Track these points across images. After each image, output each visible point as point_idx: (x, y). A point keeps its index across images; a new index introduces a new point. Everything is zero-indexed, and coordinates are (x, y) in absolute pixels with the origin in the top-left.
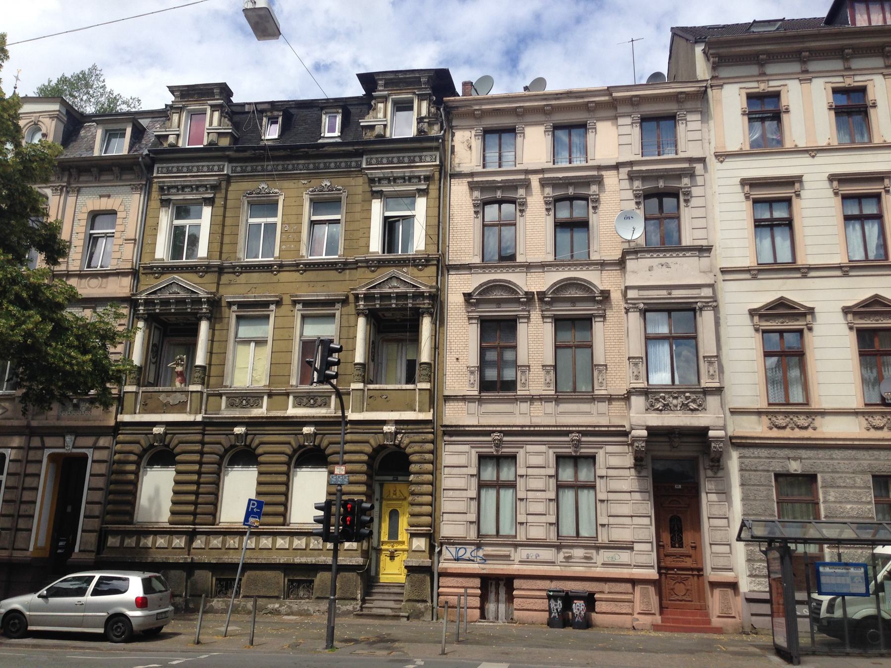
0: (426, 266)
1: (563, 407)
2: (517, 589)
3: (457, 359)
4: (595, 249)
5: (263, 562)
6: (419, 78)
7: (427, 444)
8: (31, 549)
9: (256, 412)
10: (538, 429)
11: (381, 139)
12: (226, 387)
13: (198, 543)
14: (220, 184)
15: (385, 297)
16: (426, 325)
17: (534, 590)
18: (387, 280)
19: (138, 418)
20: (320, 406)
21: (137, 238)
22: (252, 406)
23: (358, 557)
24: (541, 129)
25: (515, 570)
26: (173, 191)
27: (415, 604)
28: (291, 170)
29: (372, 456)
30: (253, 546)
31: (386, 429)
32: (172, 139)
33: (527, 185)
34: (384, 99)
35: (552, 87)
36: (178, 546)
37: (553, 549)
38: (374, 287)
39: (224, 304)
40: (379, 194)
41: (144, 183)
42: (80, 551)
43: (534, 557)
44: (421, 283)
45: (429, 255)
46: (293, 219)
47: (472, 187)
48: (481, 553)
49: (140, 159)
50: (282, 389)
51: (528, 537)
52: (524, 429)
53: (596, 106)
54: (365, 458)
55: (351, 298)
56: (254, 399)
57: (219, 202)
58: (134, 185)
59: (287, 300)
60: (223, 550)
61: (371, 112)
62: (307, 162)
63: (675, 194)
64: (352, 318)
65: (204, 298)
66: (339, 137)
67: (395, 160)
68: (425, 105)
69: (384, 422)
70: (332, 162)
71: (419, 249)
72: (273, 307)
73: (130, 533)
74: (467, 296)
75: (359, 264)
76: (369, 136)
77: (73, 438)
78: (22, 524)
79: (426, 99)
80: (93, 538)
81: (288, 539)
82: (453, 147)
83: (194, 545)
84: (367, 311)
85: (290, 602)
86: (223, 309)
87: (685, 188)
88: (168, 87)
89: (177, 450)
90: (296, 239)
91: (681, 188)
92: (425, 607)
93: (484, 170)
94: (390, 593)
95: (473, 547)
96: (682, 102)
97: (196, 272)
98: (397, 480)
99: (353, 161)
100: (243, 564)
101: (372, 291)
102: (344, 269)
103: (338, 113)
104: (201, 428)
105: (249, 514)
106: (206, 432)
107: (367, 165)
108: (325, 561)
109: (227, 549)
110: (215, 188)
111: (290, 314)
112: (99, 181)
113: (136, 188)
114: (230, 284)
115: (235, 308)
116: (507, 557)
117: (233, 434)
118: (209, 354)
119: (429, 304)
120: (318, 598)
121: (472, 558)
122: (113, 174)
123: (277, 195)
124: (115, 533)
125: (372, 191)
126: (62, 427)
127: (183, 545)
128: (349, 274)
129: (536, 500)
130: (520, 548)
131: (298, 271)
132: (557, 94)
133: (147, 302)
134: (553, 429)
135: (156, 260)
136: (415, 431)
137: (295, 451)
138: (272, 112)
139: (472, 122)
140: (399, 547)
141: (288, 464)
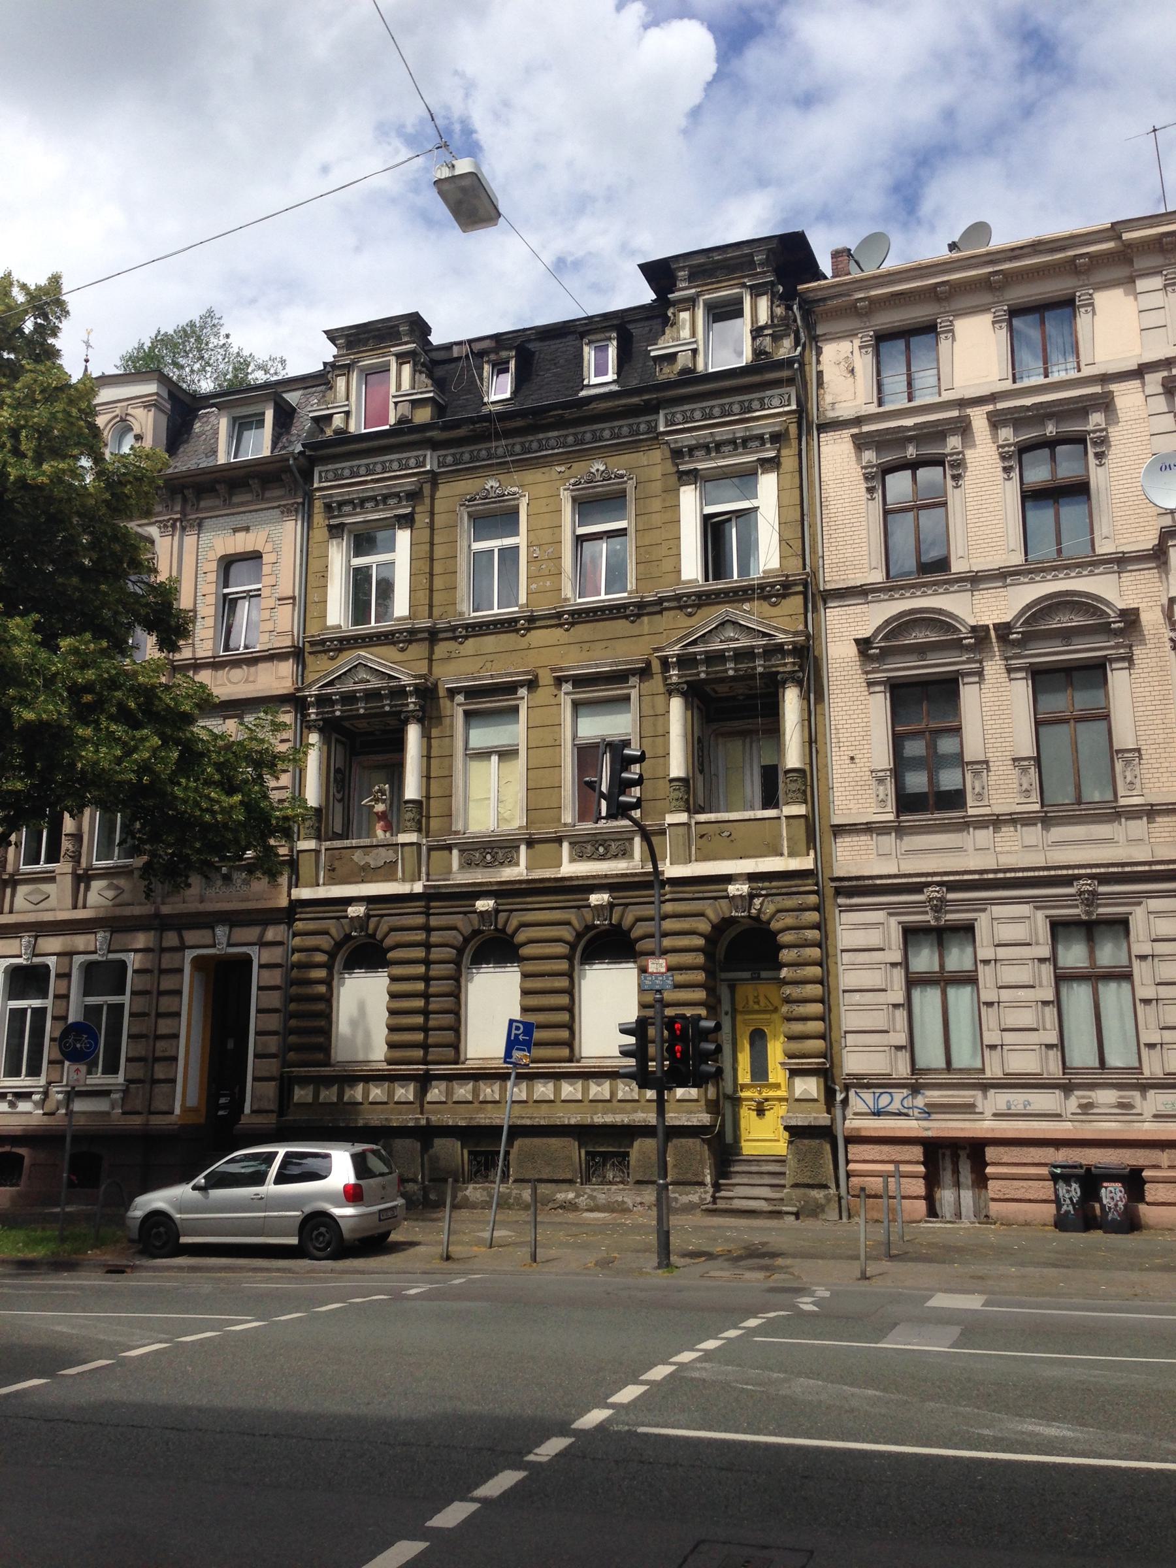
0: (784, 596)
1: (1059, 833)
3: (852, 758)
4: (1105, 532)
5: (543, 1123)
6: (751, 255)
7: (807, 913)
8: (177, 1111)
10: (1012, 875)
11: (690, 376)
12: (457, 833)
13: (435, 1093)
15: (349, 698)
16: (791, 702)
17: (1025, 1164)
19: (323, 892)
20: (615, 857)
21: (297, 594)
22: (502, 864)
24: (986, 319)
25: (987, 1130)
28: (536, 451)
30: (524, 1097)
31: (733, 889)
33: (963, 428)
36: (403, 1100)
37: (1057, 1091)
38: (331, 684)
39: (442, 693)
40: (692, 477)
41: (300, 500)
42: (253, 1112)
43: (1021, 1107)
44: (777, 629)
45: (787, 576)
47: (861, 443)
48: (920, 1101)
49: (291, 462)
50: (549, 830)
51: (1007, 1071)
52: (985, 876)
55: (656, 666)
56: (504, 851)
57: (422, 519)
58: (284, 506)
59: (546, 678)
60: (476, 1105)
64: (660, 700)
65: (409, 685)
66: (614, 381)
68: (763, 303)
69: (728, 879)
70: (605, 428)
71: (769, 567)
72: (523, 692)
73: (328, 1081)
74: (863, 644)
75: (666, 604)
76: (668, 373)
78: (160, 1072)
79: (409, 362)
81: (579, 1084)
82: (820, 374)
84: (685, 687)
85: (594, 1190)
89: (389, 942)
95: (905, 1092)
97: (394, 643)
98: (759, 978)
99: (642, 423)
100: (510, 1127)
101: (691, 650)
102: (639, 616)
103: (610, 339)
104: (423, 904)
106: (432, 911)
109: (481, 1102)
111: (553, 701)
112: (231, 506)
113: (289, 511)
114: (449, 658)
115: (460, 698)
117: (475, 912)
119: (794, 664)
120: (638, 1182)
121: (905, 1111)
123: (515, 497)
124: (304, 1081)
125: (678, 472)
127: (411, 1098)
128: (649, 622)
130: (993, 1091)
131: (561, 625)
132: (1013, 250)
133: (322, 700)
134: (1041, 873)
136: (784, 890)
137: (579, 936)
138: (497, 353)
141: (570, 958)
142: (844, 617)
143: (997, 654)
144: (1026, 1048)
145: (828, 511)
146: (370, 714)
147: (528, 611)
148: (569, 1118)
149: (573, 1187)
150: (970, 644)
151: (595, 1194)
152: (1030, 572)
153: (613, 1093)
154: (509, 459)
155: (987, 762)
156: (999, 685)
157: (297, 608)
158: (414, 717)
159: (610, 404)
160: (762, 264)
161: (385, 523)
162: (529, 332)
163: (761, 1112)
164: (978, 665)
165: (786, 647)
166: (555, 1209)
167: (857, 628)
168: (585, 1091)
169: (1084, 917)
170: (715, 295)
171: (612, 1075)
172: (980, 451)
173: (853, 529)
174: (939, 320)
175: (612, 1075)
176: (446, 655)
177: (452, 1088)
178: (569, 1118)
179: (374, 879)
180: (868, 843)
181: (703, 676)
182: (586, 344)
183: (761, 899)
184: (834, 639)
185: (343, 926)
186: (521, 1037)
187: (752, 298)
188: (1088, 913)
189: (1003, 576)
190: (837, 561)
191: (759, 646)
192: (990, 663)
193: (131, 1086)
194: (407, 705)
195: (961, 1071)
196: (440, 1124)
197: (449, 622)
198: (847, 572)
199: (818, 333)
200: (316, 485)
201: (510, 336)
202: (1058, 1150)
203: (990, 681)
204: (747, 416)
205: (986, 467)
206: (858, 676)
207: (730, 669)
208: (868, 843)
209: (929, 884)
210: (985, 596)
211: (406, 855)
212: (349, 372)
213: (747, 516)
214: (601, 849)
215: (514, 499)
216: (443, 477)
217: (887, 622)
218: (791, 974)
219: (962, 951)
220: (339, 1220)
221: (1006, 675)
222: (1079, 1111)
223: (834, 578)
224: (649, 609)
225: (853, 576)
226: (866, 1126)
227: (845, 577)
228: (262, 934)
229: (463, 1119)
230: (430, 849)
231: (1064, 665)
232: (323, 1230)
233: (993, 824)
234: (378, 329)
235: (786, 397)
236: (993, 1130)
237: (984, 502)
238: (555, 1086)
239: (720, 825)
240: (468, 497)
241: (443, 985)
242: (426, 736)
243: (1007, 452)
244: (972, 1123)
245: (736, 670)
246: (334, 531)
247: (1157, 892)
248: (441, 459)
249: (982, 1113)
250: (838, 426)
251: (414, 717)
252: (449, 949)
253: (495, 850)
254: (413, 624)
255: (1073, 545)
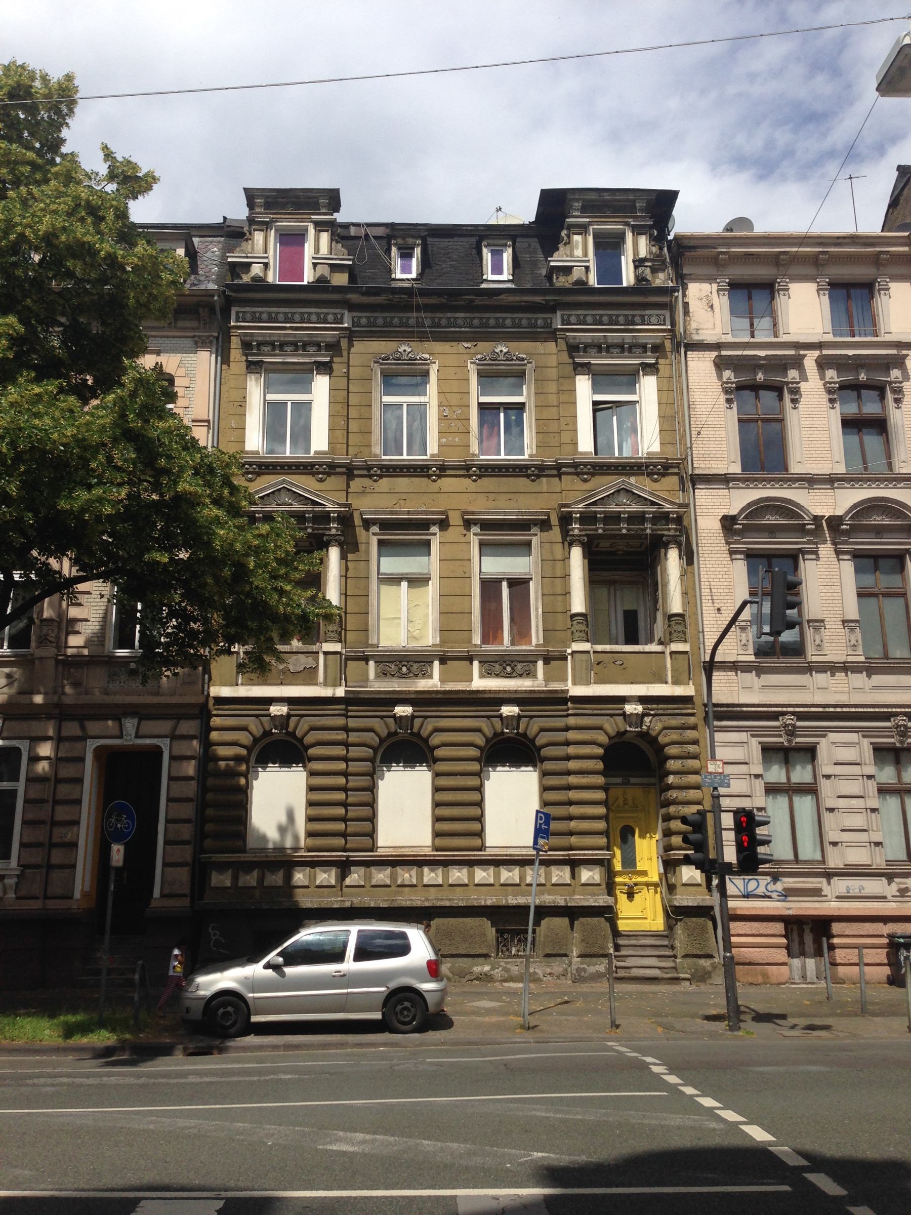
0: (663, 475)
1: (878, 679)
2: (734, 935)
3: (719, 610)
4: (903, 458)
5: (461, 904)
6: (634, 201)
7: (689, 731)
8: (77, 895)
9: (423, 684)
10: (848, 710)
12: (372, 646)
13: (355, 877)
14: (339, 342)
15: (615, 518)
16: (673, 560)
17: (862, 936)
18: (613, 494)
19: (243, 691)
20: (521, 676)
21: (211, 418)
22: (416, 676)
23: (602, 894)
24: (811, 287)
25: (834, 909)
26: (266, 349)
27: (695, 960)
28: (445, 327)
29: (608, 749)
30: (440, 881)
31: (630, 708)
32: (256, 270)
33: (797, 363)
34: (582, 229)
35: (761, 227)
36: (325, 884)
37: (883, 879)
38: (594, 504)
39: (357, 522)
40: (584, 368)
41: (216, 334)
42: (163, 896)
43: (857, 891)
44: (665, 500)
45: (667, 459)
46: (454, 399)
47: (721, 364)
48: (779, 886)
49: (216, 298)
50: (462, 649)
52: (827, 710)
53: (730, 258)
54: (600, 751)
55: (554, 520)
56: (418, 665)
57: (339, 368)
58: (199, 337)
59: (455, 519)
60: (393, 888)
61: (561, 246)
62: (468, 315)
63: (778, 389)
64: (558, 550)
65: (334, 512)
66: (509, 281)
67: (605, 319)
68: (643, 241)
69: (623, 700)
70: (508, 318)
71: (651, 450)
72: (434, 529)
73: (249, 867)
74: (728, 522)
75: (564, 470)
76: (561, 281)
77: (136, 721)
78: (57, 857)
79: (327, 231)
80: (183, 875)
81: (492, 869)
82: (686, 305)
83: (348, 881)
84: (586, 539)
85: (506, 963)
86: (357, 529)
87: (895, 383)
88: (244, 189)
90: (462, 429)
91: (787, 383)
92: (711, 964)
93: (752, 340)
94: (636, 946)
95: (769, 878)
96: (823, 265)
97: (313, 474)
98: (628, 783)
99: (540, 318)
100: (536, 907)
101: (593, 509)
102: (538, 477)
103: (505, 245)
104: (343, 707)
105: (539, 832)
106: (349, 714)
107: (563, 325)
108: (554, 902)
109: (399, 886)
110: (333, 348)
111: (463, 539)
114: (363, 492)
115: (375, 529)
116: (816, 892)
117: (269, 715)
118: (343, 596)
119: (676, 530)
120: (548, 956)
122: (199, 320)
123: (426, 363)
124: (222, 867)
125: (574, 363)
126: (117, 706)
127: (333, 882)
128: (548, 483)
129: (851, 811)
130: (836, 878)
131: (470, 476)
132: (838, 238)
134: (869, 710)
135: (247, 453)
136: (669, 712)
137: (256, 740)
138: (404, 239)
139: (710, 270)
140: (640, 879)
141: (372, 760)
142: (709, 497)
143: (828, 539)
144: (859, 845)
145: (695, 413)
146: (607, 535)
147: (441, 461)
148: (485, 900)
149: (488, 960)
150: (811, 529)
151: (509, 966)
152: (852, 480)
153: (522, 878)
154: (416, 329)
155: (823, 621)
156: (830, 563)
157: (211, 431)
158: (580, 541)
159: (517, 298)
160: (641, 210)
161: (305, 367)
162: (421, 227)
163: (630, 895)
164: (815, 546)
165: (332, 515)
166: (472, 980)
167: (720, 507)
168: (497, 876)
169: (898, 745)
170: (602, 227)
171: (523, 862)
172: (811, 383)
173: (715, 429)
174: (778, 280)
175: (523, 862)
176: (361, 490)
177: (371, 874)
178: (485, 900)
179: (293, 682)
180: (733, 677)
181: (600, 531)
182: (486, 246)
183: (650, 717)
184: (702, 514)
185: (262, 724)
186: (543, 826)
187: (633, 235)
188: (901, 742)
189: (831, 481)
190: (703, 452)
191: (649, 513)
192: (822, 546)
193: (27, 871)
194: (330, 529)
195: (806, 862)
196: (362, 905)
197: (366, 461)
198: (711, 462)
199: (684, 272)
200: (232, 324)
201: (404, 227)
202: (885, 924)
203: (824, 559)
204: (631, 327)
205: (815, 396)
206: (722, 545)
207: (624, 529)
208: (733, 677)
209: (784, 714)
210: (817, 494)
211: (329, 662)
212: (267, 229)
213: (308, 405)
214: (509, 669)
215: (424, 364)
216: (358, 335)
217: (749, 505)
218: (677, 780)
219: (804, 768)
220: (425, 995)
221: (835, 556)
222: (898, 894)
223: (701, 466)
224: (547, 472)
225: (716, 466)
226: (739, 906)
227: (710, 466)
228: (175, 728)
229: (384, 900)
230: (347, 659)
231: (874, 553)
232: (407, 1004)
233: (866, 671)
234: (298, 197)
235: (662, 318)
236: (839, 909)
237: (814, 422)
238: (468, 872)
239: (613, 655)
240: (383, 356)
241: (361, 780)
242: (343, 557)
243: (833, 388)
244: (820, 903)
245: (628, 530)
246: (252, 367)
247: (834, 728)
248: (356, 320)
249: (826, 896)
250: (699, 347)
251: (336, 541)
252: (366, 749)
253: (410, 663)
254: (333, 459)
255: (877, 464)
